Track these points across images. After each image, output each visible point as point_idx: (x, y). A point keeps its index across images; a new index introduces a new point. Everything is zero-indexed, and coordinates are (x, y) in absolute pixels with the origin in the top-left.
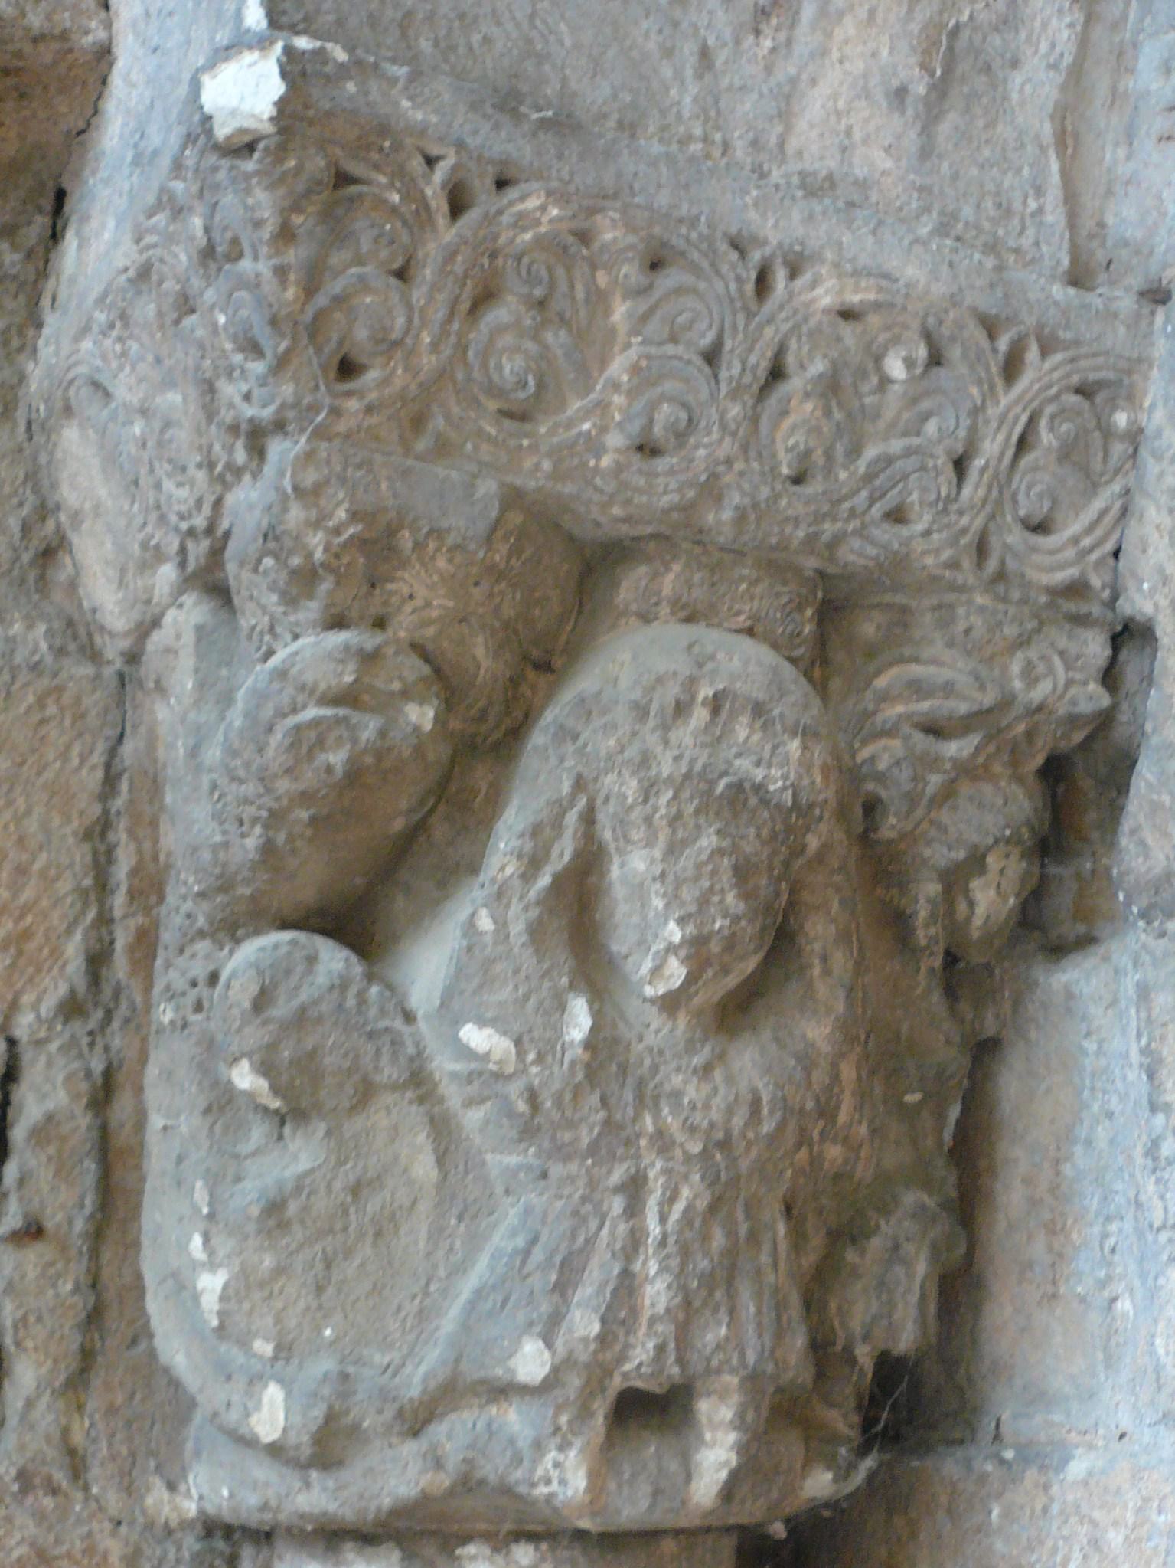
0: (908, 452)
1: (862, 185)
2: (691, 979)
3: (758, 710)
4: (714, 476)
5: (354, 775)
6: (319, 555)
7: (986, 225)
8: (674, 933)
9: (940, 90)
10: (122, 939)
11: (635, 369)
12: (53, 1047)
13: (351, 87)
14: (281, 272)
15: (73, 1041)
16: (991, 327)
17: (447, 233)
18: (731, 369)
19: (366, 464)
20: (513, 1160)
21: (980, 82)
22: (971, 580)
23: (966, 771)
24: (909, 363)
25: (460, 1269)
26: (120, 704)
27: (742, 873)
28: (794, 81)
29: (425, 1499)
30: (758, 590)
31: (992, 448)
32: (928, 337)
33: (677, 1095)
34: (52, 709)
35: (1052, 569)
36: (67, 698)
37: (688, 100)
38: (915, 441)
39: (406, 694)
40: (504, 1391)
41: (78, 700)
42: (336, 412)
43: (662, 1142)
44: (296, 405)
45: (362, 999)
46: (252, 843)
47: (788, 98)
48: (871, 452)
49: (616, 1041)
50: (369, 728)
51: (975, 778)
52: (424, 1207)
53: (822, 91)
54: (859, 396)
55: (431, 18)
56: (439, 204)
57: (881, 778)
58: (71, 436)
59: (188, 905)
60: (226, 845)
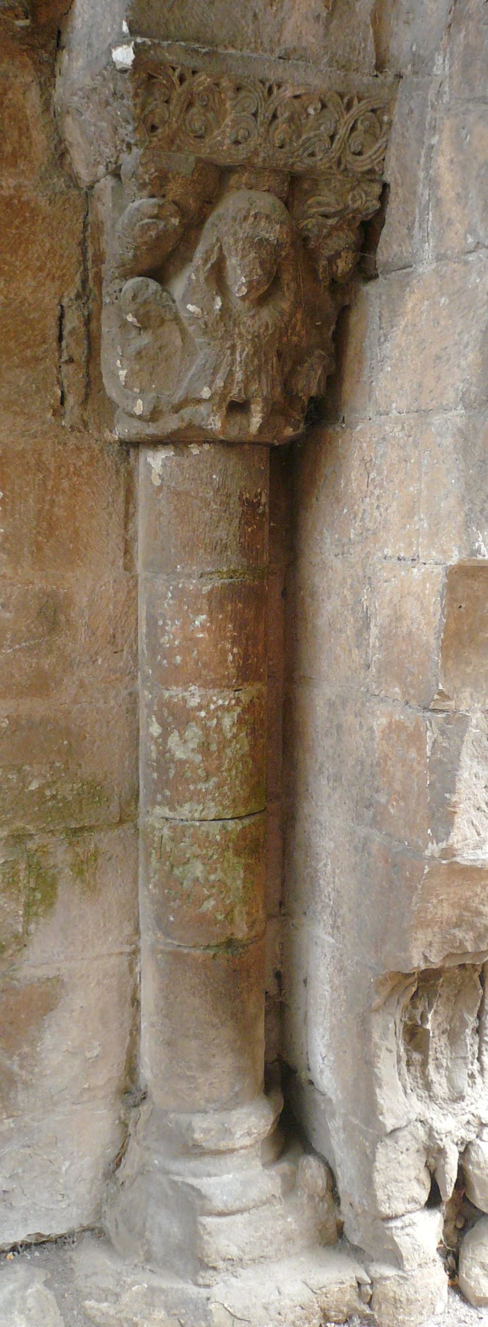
0: (315, 136)
1: (305, 49)
2: (248, 292)
3: (267, 217)
4: (256, 149)
5: (158, 237)
6: (147, 181)
7: (346, 55)
8: (244, 280)
9: (331, 14)
10: (91, 275)
11: (233, 121)
12: (73, 308)
13: (152, 52)
14: (135, 105)
15: (79, 306)
16: (341, 96)
17: (179, 90)
18: (260, 118)
19: (159, 156)
20: (202, 340)
21: (346, 8)
22: (336, 172)
23: (334, 228)
24: (315, 109)
25: (188, 369)
26: (87, 203)
27: (262, 264)
28: (283, 19)
29: (179, 429)
30: (271, 179)
31: (342, 132)
32: (321, 101)
33: (245, 323)
34: (67, 206)
35: (362, 166)
36: (71, 202)
37: (250, 31)
38: (318, 132)
39: (171, 216)
40: (200, 401)
41: (74, 202)
42: (151, 142)
43: (241, 336)
44: (140, 141)
45: (161, 296)
46: (131, 254)
47: (281, 25)
48: (304, 137)
49: (228, 308)
50: (161, 225)
51: (337, 230)
52: (179, 353)
53: (293, 20)
54: (300, 120)
55: (173, 20)
56: (175, 79)
57: (309, 230)
58: (69, 120)
59: (112, 270)
60: (123, 254)
